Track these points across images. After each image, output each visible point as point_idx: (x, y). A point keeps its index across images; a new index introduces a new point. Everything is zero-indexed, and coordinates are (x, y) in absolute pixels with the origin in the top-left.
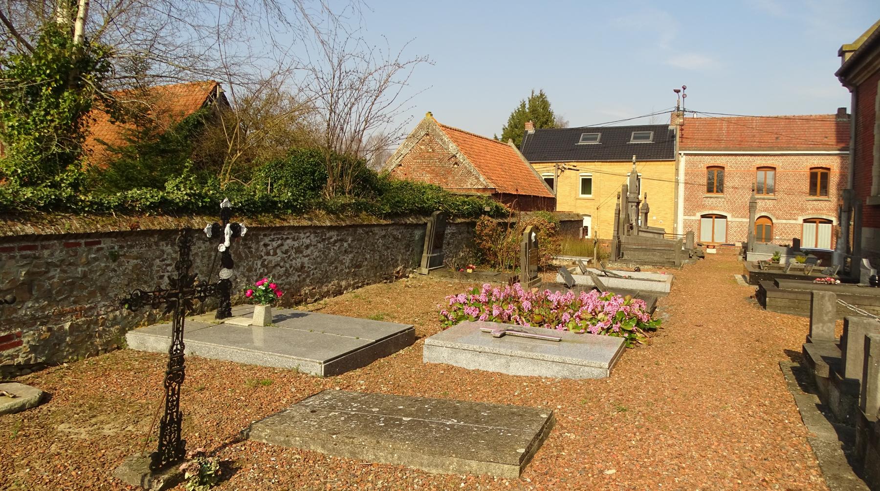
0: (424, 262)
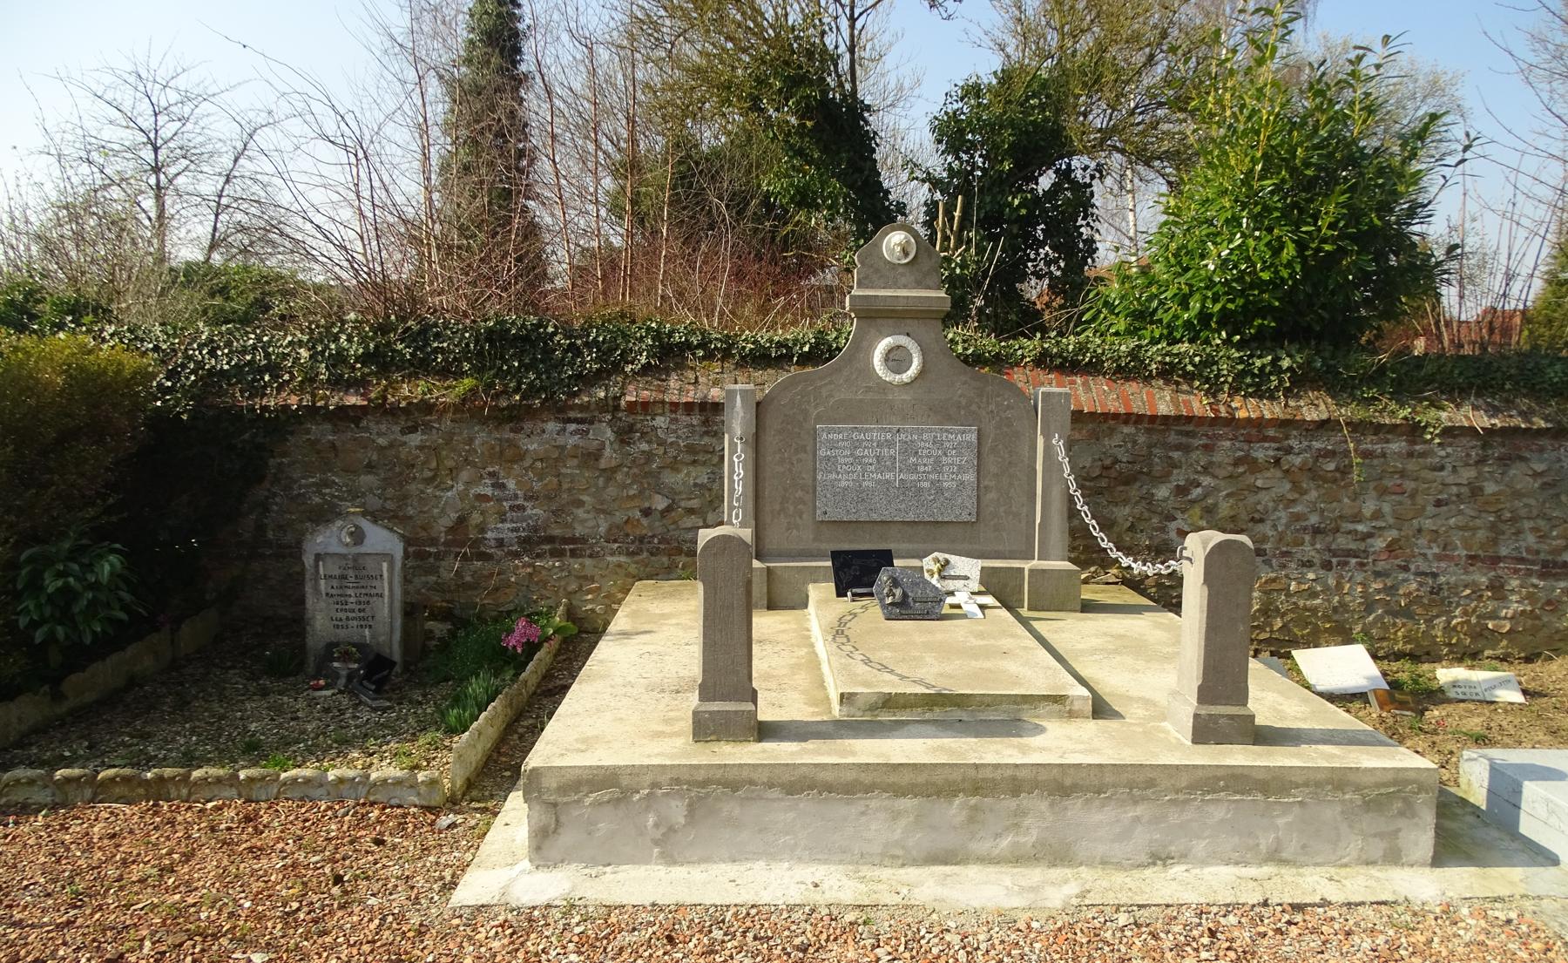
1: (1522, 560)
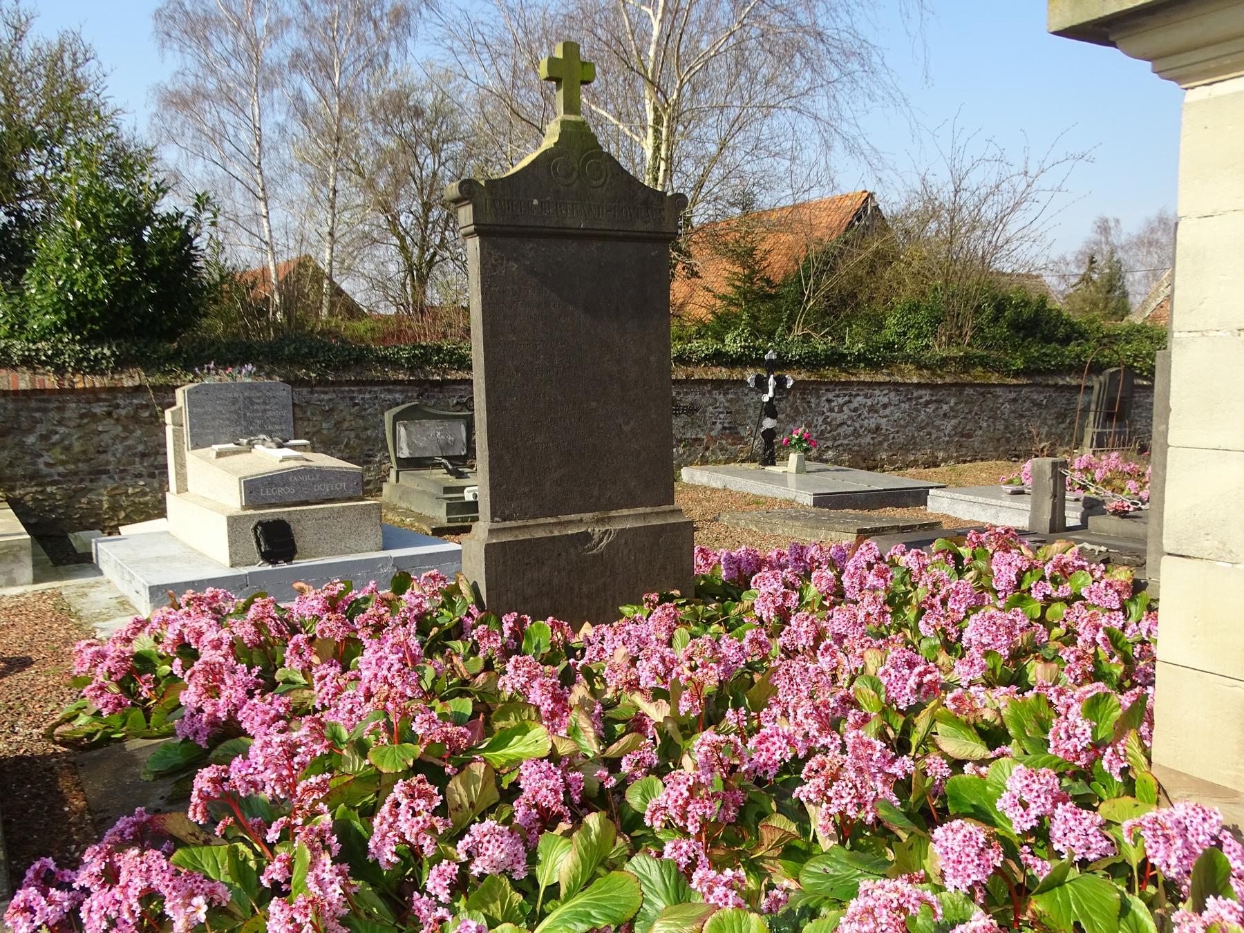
0: (1087, 440)
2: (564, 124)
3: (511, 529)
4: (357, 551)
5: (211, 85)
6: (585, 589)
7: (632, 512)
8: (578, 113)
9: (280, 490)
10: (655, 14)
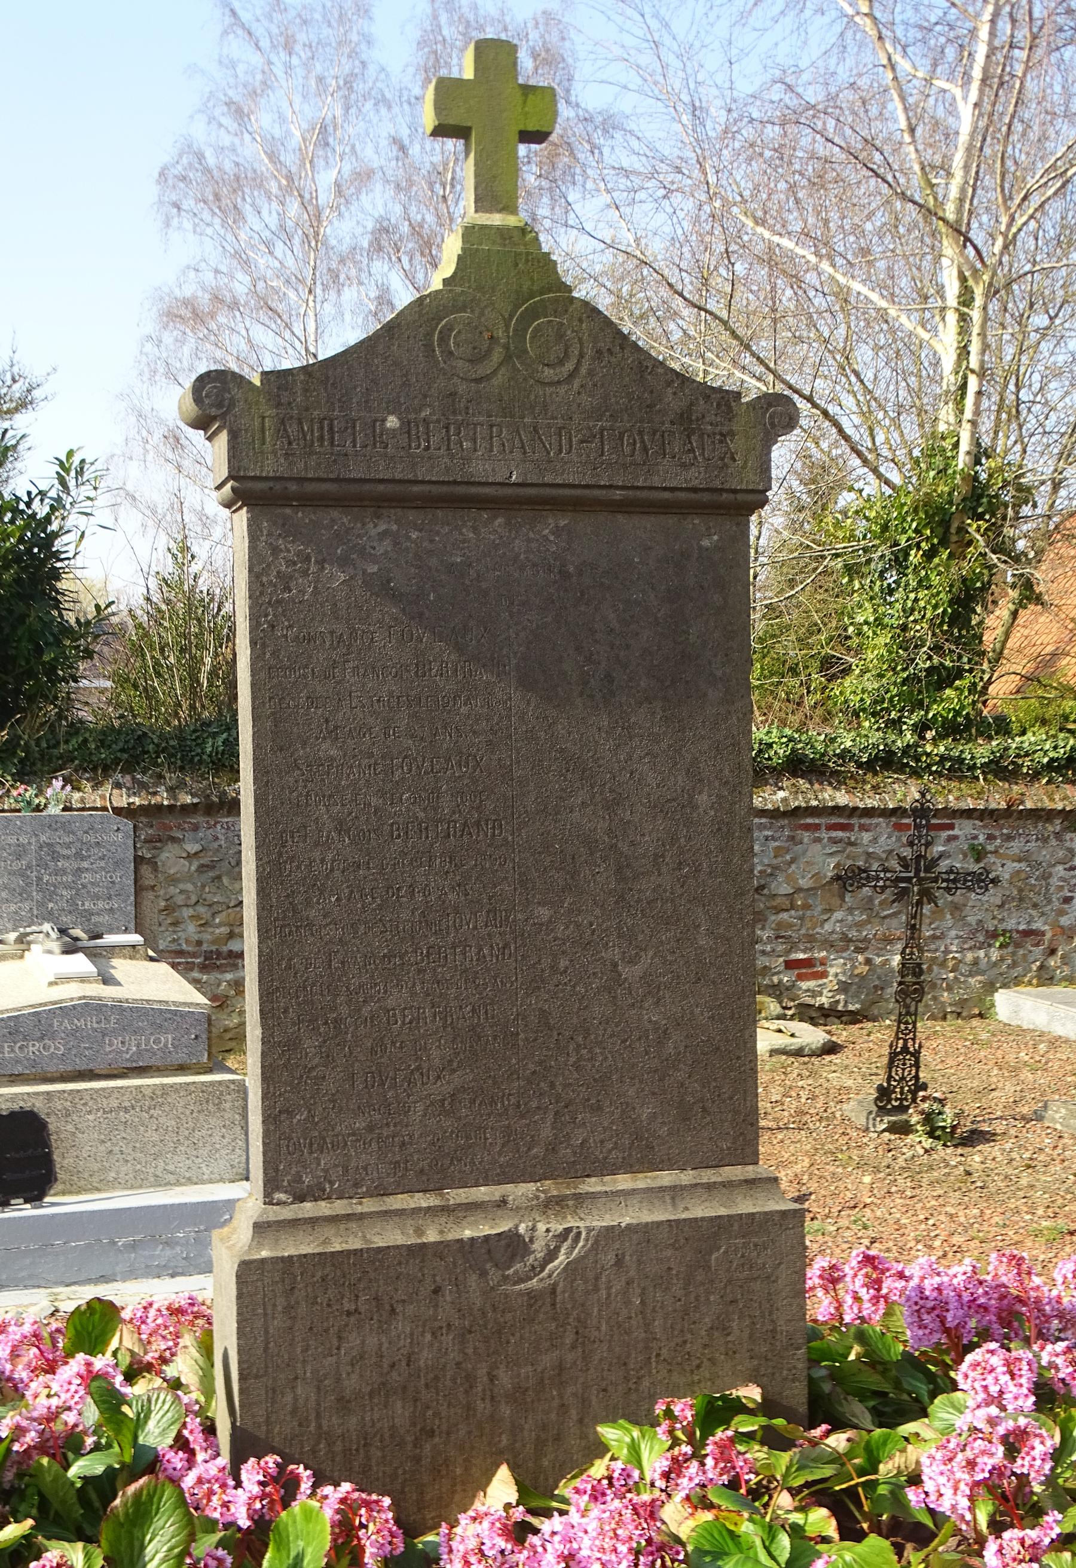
1: (180, 953)
2: (470, 233)
3: (313, 1222)
4: (190, 1181)
5: (241, 286)
6: (505, 1379)
7: (642, 1181)
8: (510, 208)
9: (34, 1048)
10: (965, 98)
